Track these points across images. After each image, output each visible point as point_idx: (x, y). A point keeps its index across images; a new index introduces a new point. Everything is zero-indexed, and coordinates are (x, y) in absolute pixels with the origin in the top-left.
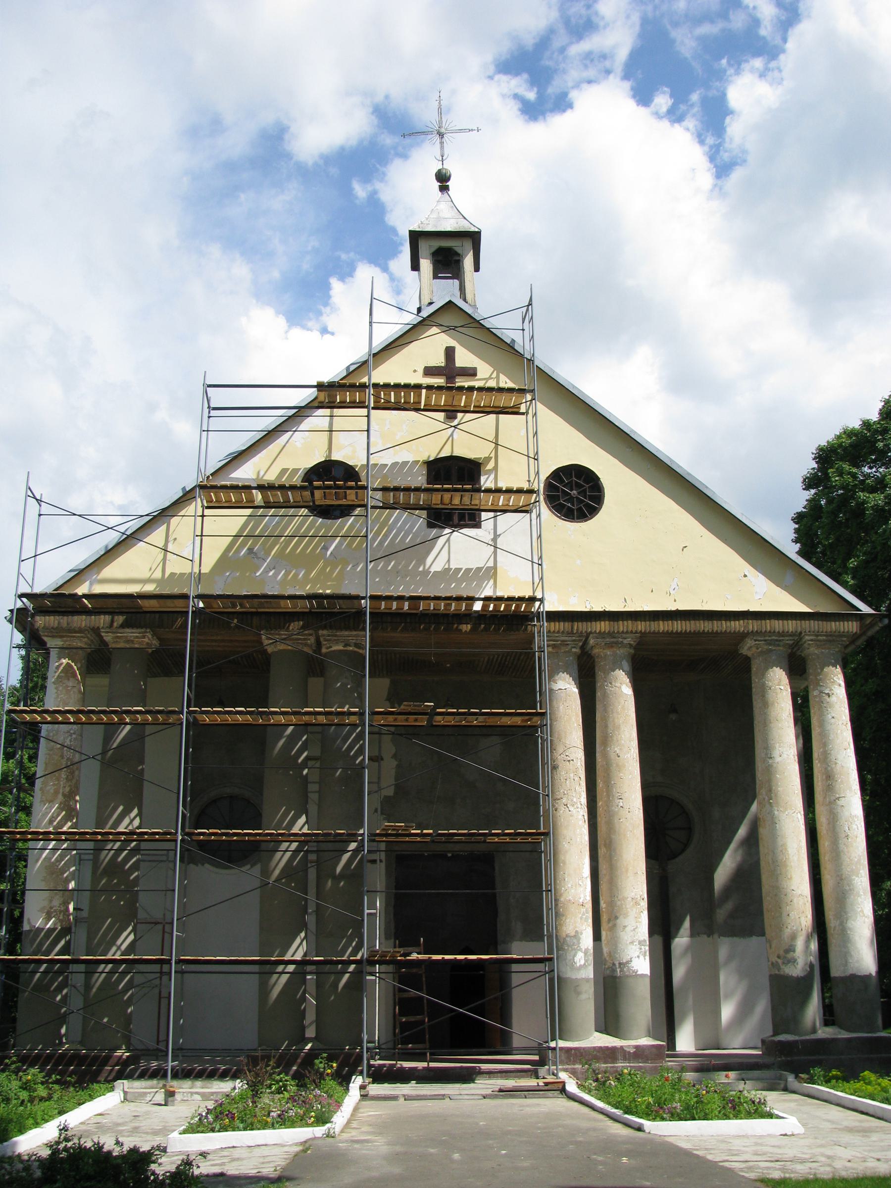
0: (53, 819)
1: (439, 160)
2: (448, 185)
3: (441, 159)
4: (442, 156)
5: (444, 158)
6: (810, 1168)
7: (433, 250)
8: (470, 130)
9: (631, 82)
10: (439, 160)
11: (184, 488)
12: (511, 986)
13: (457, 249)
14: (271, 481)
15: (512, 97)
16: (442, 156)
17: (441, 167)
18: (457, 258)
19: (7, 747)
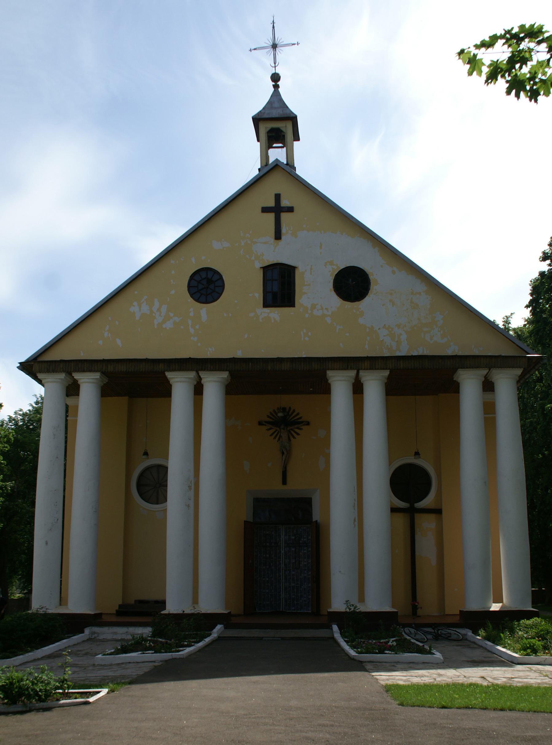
0: (443, 675)
1: (273, 67)
2: (278, 85)
3: (274, 66)
4: (275, 64)
5: (276, 65)
6: (422, 680)
7: (268, 129)
8: (292, 45)
9: (39, 390)
10: (273, 67)
11: (275, 23)
12: (202, 370)
13: (282, 129)
14: (257, 175)
15: (66, 397)
16: (275, 64)
17: (274, 72)
18: (284, 134)
19: (31, 589)
